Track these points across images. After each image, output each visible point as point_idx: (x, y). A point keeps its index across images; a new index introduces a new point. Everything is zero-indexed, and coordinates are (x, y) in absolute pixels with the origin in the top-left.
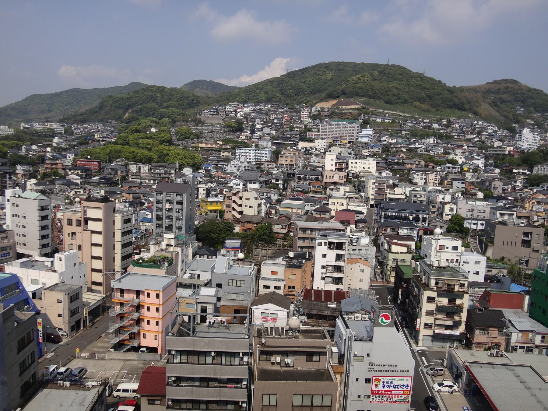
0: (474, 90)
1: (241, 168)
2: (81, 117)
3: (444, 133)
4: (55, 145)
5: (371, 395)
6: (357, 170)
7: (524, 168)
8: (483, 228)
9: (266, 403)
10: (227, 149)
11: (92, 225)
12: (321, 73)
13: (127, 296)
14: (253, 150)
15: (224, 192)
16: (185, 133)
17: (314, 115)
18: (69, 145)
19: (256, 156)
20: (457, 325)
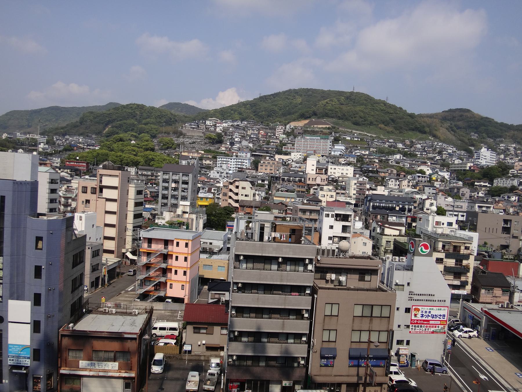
0: (431, 116)
1: (223, 175)
2: (62, 131)
3: (408, 151)
4: (41, 150)
5: (411, 325)
6: (337, 175)
7: (485, 181)
8: (465, 220)
9: (328, 313)
10: (208, 158)
11: (106, 193)
12: (291, 98)
13: (154, 247)
14: (234, 159)
15: (213, 191)
16: (168, 143)
17: (288, 132)
18: (55, 151)
19: (236, 165)
20: (463, 285)
